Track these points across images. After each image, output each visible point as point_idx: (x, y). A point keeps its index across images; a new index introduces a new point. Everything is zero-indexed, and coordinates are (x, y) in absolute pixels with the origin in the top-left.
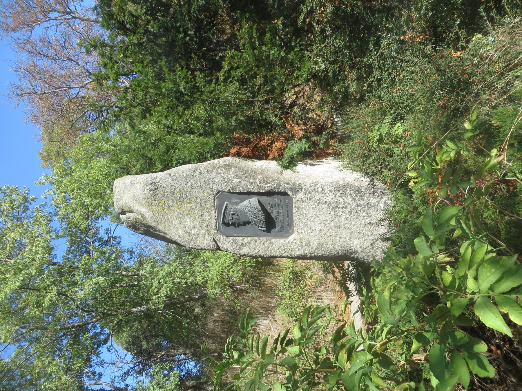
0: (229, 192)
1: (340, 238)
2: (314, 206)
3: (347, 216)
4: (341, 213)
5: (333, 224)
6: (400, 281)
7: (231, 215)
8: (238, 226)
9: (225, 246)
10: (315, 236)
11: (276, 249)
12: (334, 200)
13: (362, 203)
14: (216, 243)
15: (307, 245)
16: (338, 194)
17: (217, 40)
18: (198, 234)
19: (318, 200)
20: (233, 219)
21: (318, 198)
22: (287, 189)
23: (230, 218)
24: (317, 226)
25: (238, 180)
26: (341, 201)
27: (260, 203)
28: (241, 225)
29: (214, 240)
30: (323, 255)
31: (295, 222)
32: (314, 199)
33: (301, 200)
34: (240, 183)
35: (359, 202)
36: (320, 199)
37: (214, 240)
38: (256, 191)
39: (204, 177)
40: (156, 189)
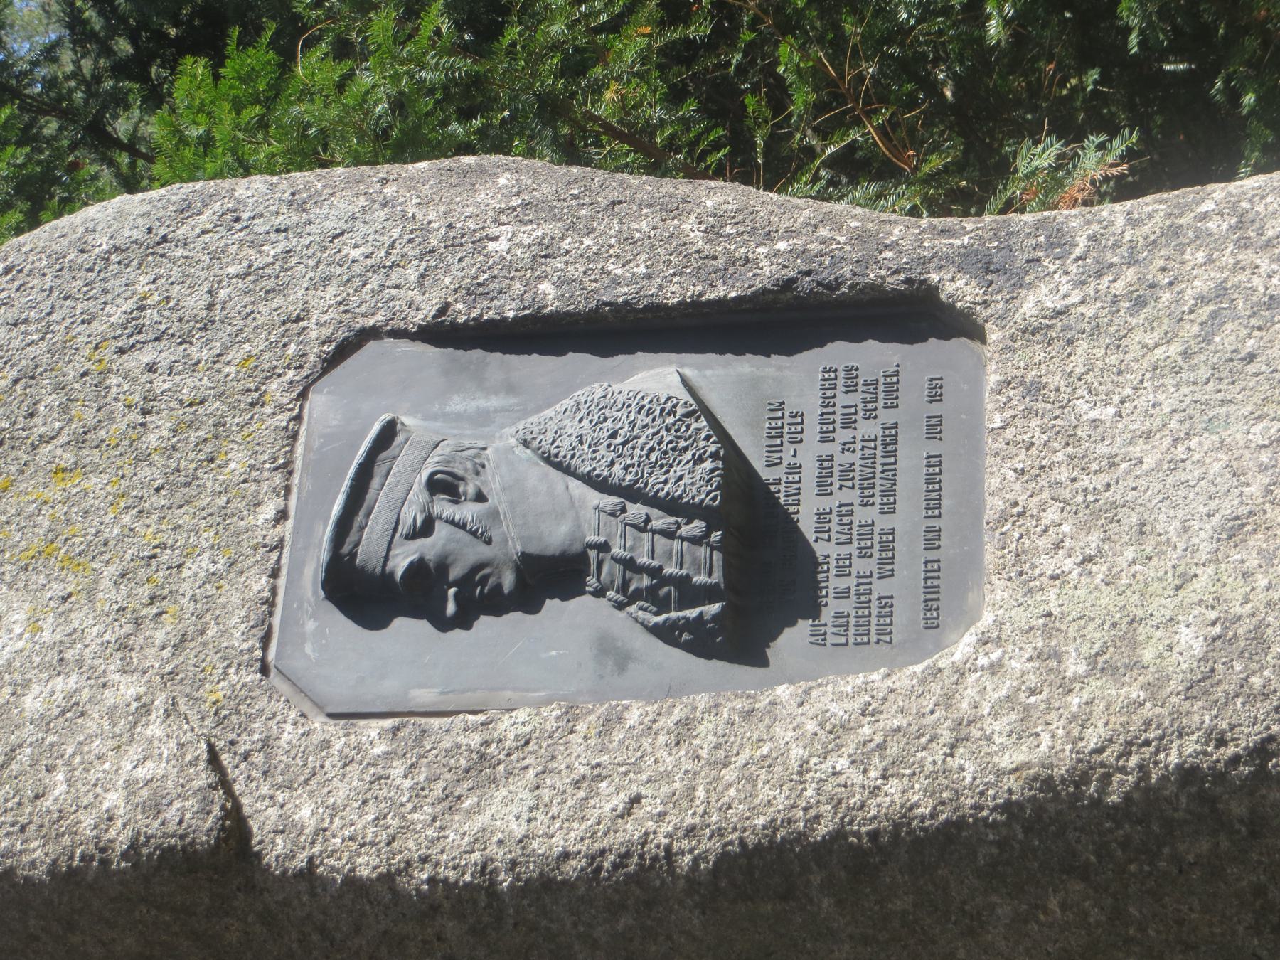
2: (1174, 349)
7: (418, 494)
8: (464, 620)
9: (305, 813)
10: (1186, 579)
11: (797, 752)
14: (225, 783)
15: (1110, 670)
18: (73, 709)
19: (1202, 300)
20: (425, 528)
22: (945, 261)
23: (411, 514)
25: (530, 234)
27: (685, 381)
28: (497, 604)
29: (214, 759)
34: (546, 251)
36: (1221, 291)
37: (214, 759)
38: (675, 291)
39: (256, 245)
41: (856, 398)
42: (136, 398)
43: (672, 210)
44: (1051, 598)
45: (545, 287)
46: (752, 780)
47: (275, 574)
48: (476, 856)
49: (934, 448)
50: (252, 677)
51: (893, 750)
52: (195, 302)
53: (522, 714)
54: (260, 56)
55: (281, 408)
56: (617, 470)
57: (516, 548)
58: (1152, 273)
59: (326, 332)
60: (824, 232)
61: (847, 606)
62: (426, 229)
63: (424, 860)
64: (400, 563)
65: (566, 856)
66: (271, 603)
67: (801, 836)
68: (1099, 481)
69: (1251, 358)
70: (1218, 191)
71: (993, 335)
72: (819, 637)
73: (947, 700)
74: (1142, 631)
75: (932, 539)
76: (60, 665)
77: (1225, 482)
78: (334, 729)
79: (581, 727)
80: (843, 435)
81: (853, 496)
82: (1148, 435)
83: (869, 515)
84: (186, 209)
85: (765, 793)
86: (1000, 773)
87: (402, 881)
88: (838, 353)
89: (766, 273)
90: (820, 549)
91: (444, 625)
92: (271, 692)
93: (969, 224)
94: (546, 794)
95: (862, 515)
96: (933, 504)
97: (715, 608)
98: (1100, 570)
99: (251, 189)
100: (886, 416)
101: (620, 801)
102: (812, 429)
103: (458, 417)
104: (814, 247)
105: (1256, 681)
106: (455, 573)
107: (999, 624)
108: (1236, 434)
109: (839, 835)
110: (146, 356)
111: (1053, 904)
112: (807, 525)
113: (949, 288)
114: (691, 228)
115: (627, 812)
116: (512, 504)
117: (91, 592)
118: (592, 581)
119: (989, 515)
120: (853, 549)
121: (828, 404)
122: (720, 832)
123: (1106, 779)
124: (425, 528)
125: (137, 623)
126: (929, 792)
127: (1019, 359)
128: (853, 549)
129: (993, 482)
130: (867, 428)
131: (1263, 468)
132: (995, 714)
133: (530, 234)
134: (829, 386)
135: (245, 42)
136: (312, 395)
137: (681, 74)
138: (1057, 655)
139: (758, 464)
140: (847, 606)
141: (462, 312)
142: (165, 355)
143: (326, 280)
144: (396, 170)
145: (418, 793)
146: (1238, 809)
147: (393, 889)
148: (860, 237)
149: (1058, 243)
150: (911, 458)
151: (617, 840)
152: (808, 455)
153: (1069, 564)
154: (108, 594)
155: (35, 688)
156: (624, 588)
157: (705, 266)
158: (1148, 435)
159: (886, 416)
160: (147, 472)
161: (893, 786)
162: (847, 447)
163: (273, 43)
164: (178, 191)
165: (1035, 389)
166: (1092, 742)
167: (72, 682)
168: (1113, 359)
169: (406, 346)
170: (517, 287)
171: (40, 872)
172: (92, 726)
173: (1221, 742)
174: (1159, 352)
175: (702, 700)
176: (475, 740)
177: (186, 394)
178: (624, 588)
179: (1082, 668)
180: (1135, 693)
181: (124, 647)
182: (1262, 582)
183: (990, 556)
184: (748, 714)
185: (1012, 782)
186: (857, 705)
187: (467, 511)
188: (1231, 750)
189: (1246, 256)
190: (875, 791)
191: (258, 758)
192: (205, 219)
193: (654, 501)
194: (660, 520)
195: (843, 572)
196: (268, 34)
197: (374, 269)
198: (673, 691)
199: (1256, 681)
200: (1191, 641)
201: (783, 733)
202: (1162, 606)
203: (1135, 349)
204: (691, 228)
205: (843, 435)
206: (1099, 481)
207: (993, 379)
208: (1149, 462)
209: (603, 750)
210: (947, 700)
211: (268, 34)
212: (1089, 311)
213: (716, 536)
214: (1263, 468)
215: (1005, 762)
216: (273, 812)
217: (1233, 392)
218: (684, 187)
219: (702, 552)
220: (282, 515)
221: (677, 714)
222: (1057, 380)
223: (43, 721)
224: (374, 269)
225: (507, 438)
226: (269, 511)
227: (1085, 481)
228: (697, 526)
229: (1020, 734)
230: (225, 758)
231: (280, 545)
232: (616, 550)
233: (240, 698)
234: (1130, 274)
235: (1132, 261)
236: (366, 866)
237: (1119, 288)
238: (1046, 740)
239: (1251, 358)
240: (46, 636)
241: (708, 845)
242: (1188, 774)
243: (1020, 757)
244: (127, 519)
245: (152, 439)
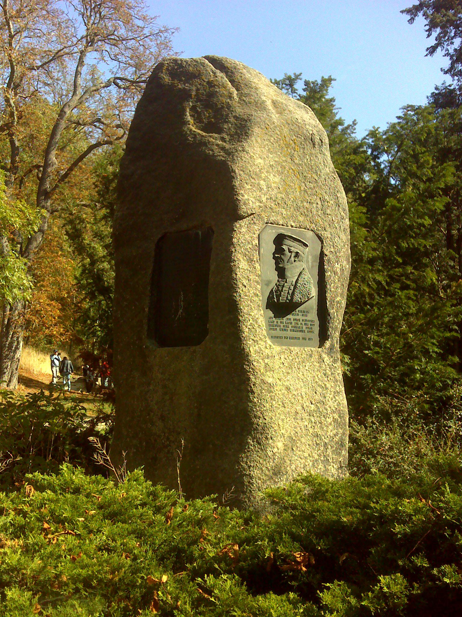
1: (283, 420)
2: (318, 381)
4: (313, 421)
5: (299, 408)
7: (296, 250)
10: (280, 380)
11: (253, 314)
12: (329, 409)
13: (329, 451)
15: (266, 367)
16: (336, 416)
18: (261, 189)
19: (325, 385)
20: (290, 251)
21: (328, 386)
23: (292, 249)
25: (338, 270)
28: (277, 264)
30: (253, 392)
32: (326, 379)
33: (321, 360)
34: (336, 273)
35: (330, 447)
36: (327, 388)
38: (328, 295)
40: (314, 144)
41: (309, 326)
42: (312, 201)
43: (342, 295)
44: (277, 357)
45: (329, 273)
46: (248, 306)
47: (283, 225)
48: (236, 259)
49: (301, 338)
50: (266, 221)
51: (253, 330)
52: (328, 212)
53: (259, 267)
54: (364, 221)
55: (310, 227)
56: (299, 285)
57: (286, 267)
58: (330, 377)
59: (323, 235)
60: (338, 321)
61: (275, 323)
62: (340, 252)
63: (236, 250)
64: (284, 247)
65: (236, 274)
66: (278, 224)
67: (239, 314)
68: (296, 366)
69: (316, 393)
70: (343, 389)
71: (320, 349)
72: (271, 318)
73: (261, 339)
74: (272, 372)
75: (286, 338)
76: (268, 187)
77: (296, 388)
78: (256, 236)
79: (257, 278)
80: (303, 323)
81: (293, 324)
82: (303, 375)
83: (290, 328)
84: (344, 210)
85: (246, 308)
86: (249, 348)
87: (232, 246)
88: (317, 323)
89: (331, 311)
90: (285, 319)
91: (274, 254)
92: (263, 224)
93: (338, 346)
94: (246, 271)
95: (290, 326)
96: (291, 338)
97: (276, 300)
98: (282, 366)
99: (347, 222)
100: (306, 331)
101: (245, 284)
102: (304, 318)
103: (308, 257)
104: (335, 319)
105: (264, 391)
106: (282, 256)
107: (273, 348)
108: (303, 390)
109: (239, 320)
110: (319, 203)
111: (227, 356)
112: (288, 317)
113: (328, 342)
114: (338, 299)
115: (243, 285)
116: (293, 266)
117: (280, 193)
118: (280, 280)
119: (290, 348)
120: (285, 324)
121: (309, 321)
122: (240, 300)
123: (248, 366)
124: (290, 251)
125: (275, 201)
126: (246, 336)
127: (316, 354)
128: (285, 324)
129: (296, 348)
130: (304, 327)
131: (298, 394)
132: (259, 347)
133: (338, 270)
134: (311, 321)
135: (367, 218)
136: (312, 232)
137: (359, 297)
138: (268, 358)
139: (299, 309)
140: (275, 323)
141: (326, 258)
142: (319, 206)
143: (332, 235)
144: (349, 247)
145: (246, 249)
146: (243, 387)
147: (231, 245)
148: (336, 328)
149: (335, 361)
150: (299, 334)
151: (239, 283)
152: (300, 317)
153: (282, 360)
154: (279, 196)
155: (264, 183)
156: (279, 285)
157: (332, 301)
158: (303, 375)
159: (306, 331)
160: (300, 203)
161: (247, 330)
162: (301, 324)
163: (367, 223)
164: (347, 208)
165: (311, 356)
166: (254, 363)
167: (265, 189)
168: (316, 370)
169: (320, 248)
170: (329, 268)
171: (234, 183)
172: (258, 193)
173: (254, 385)
174: (317, 377)
175: (261, 298)
176: (255, 259)
177: (312, 210)
178: (279, 285)
179: (266, 362)
180: (262, 371)
181: (271, 198)
182: (280, 393)
183: (284, 347)
184: (259, 306)
185: (248, 350)
186: (260, 324)
187: (293, 259)
188: (253, 387)
189: (333, 393)
190: (246, 327)
191: (252, 222)
192: (342, 213)
193: (294, 291)
194: (290, 292)
195: (281, 322)
196: (368, 222)
197: (333, 243)
198: (262, 294)
199: (264, 391)
200: (270, 380)
201: (256, 312)
202: (276, 376)
203: (317, 373)
204: (338, 299)
205: (303, 323)
206: (296, 366)
207: (312, 349)
208: (299, 375)
209: (254, 281)
210: (261, 339)
211: (368, 222)
212: (324, 366)
213: (288, 301)
214: (298, 394)
215: (251, 349)
216: (243, 224)
217: (310, 390)
218: (345, 297)
219: (285, 299)
220: (292, 226)
221: (259, 294)
222: (312, 360)
223: (259, 184)
224: (333, 243)
225: (304, 266)
226: (293, 224)
227: (296, 364)
228: (289, 298)
229: (256, 352)
230: (252, 216)
231: (287, 226)
232: (286, 284)
233: (262, 219)
234: (330, 373)
235: (332, 374)
236: (235, 240)
237: (327, 371)
238: (255, 356)
239: (316, 393)
240: (273, 185)
241: (238, 298)
242: (249, 379)
243: (252, 351)
244: (292, 199)
245: (305, 204)
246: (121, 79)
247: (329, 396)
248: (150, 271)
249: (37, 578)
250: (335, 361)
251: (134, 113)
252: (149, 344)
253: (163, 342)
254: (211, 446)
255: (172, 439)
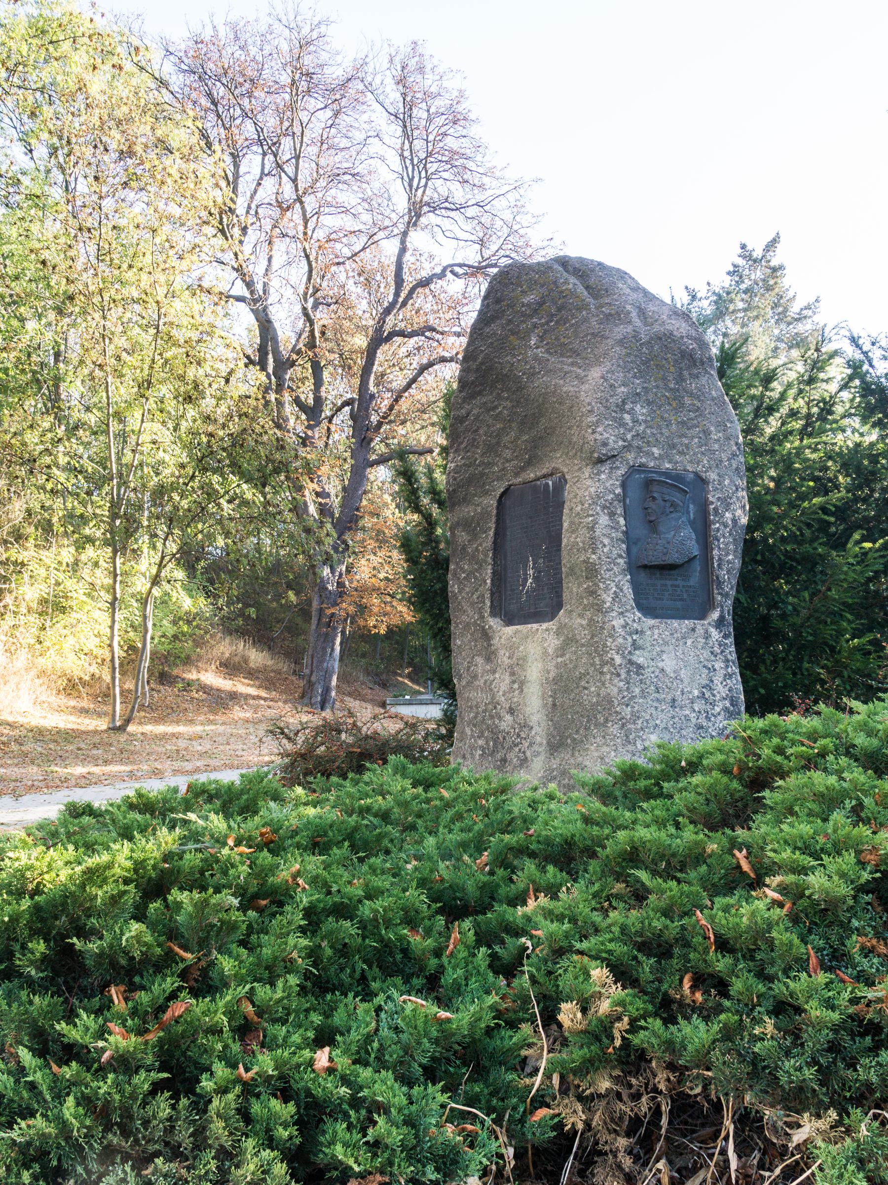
0: (705, 503)
3: (694, 721)
6: (122, 151)
17: (774, 545)
21: (717, 666)
24: (669, 663)
26: (717, 709)
31: (669, 621)
36: (715, 670)
130: (685, 596)
223: (621, 419)
246: (461, 265)
247: (718, 679)
248: (492, 533)
249: (438, 758)
250: (726, 636)
251: (464, 340)
252: (494, 623)
253: (509, 622)
254: (569, 741)
255: (523, 735)
